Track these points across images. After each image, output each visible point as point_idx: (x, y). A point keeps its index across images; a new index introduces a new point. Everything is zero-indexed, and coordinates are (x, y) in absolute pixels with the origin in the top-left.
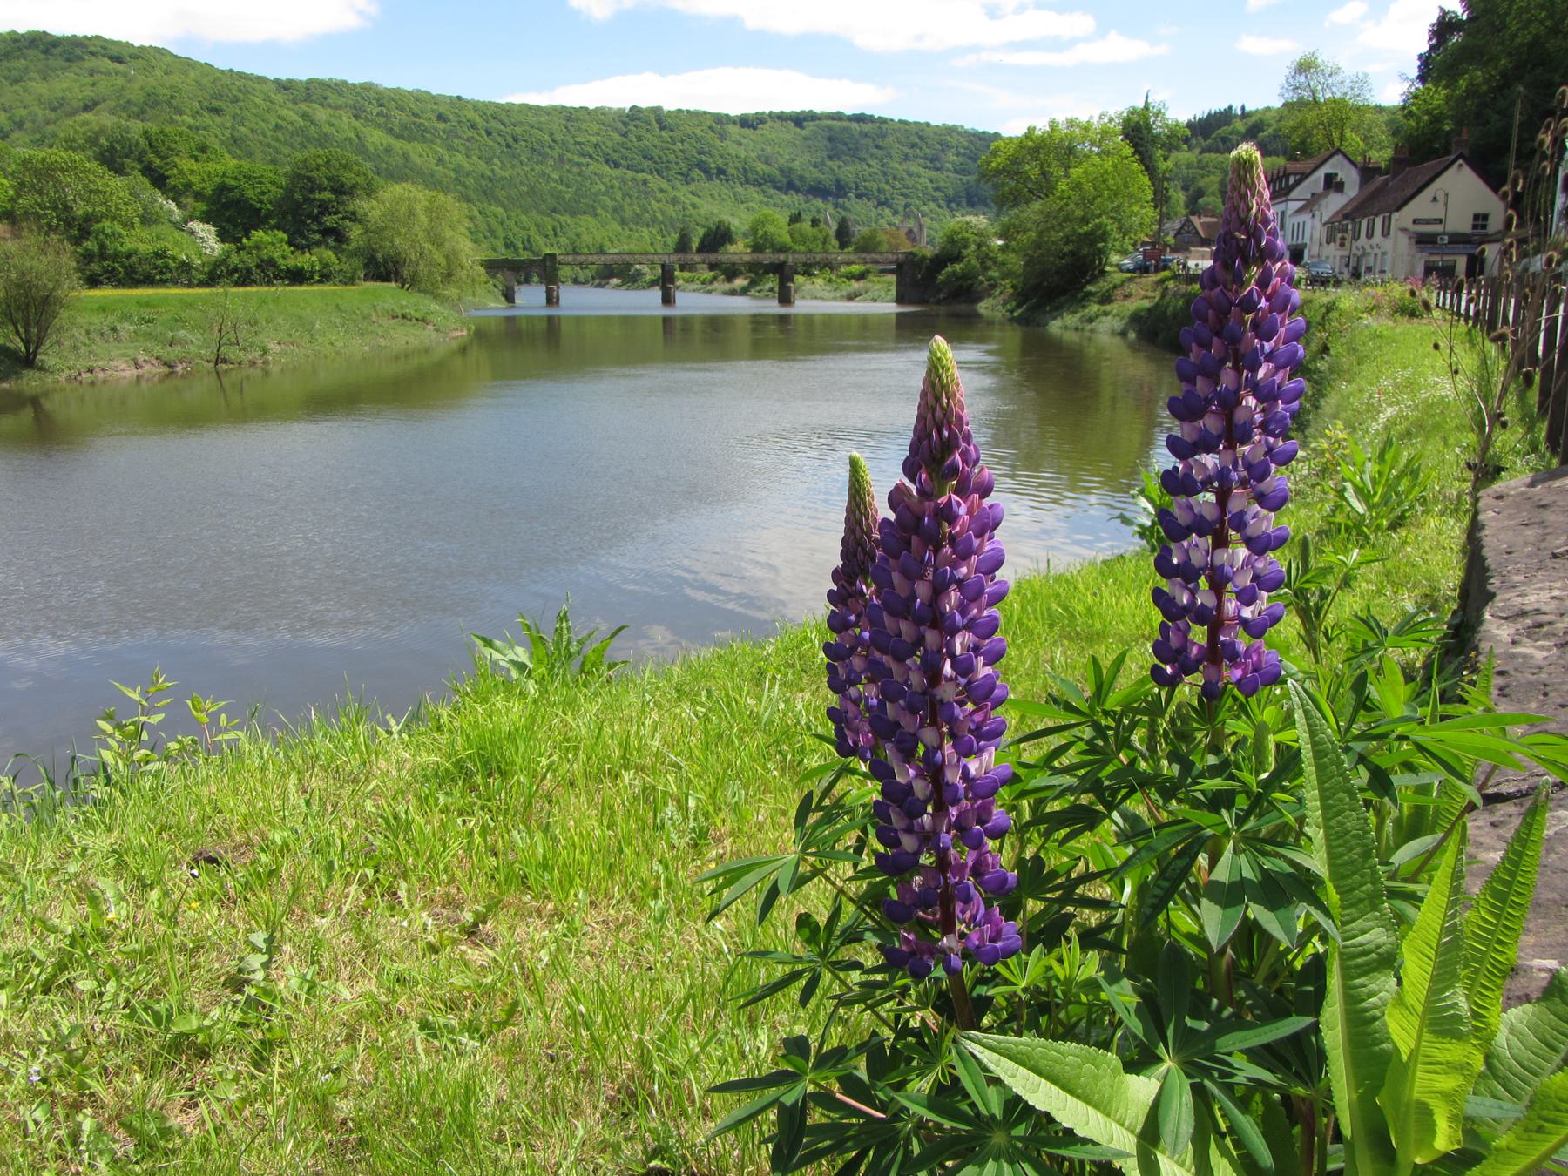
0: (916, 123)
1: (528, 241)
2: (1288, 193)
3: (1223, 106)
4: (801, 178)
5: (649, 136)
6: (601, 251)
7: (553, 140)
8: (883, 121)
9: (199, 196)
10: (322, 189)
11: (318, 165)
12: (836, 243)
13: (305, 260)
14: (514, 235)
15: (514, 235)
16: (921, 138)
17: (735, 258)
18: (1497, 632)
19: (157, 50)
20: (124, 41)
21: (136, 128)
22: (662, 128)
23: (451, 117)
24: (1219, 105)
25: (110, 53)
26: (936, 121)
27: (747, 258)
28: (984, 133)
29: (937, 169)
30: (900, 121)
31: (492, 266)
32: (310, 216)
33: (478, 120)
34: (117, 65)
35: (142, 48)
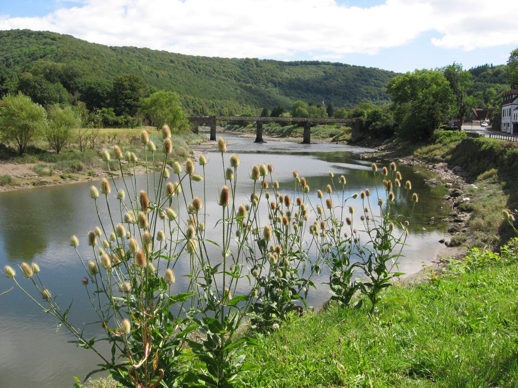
0: (359, 67)
1: (203, 109)
2: (512, 102)
3: (484, 64)
4: (312, 87)
5: (252, 69)
6: (231, 114)
7: (214, 70)
8: (346, 66)
9: (81, 91)
10: (126, 90)
11: (126, 80)
12: (327, 114)
13: (121, 119)
14: (197, 107)
15: (197, 107)
16: (361, 72)
17: (286, 119)
18: (366, 116)
19: (68, 36)
20: (57, 32)
21: (60, 66)
22: (257, 67)
23: (176, 61)
24: (482, 63)
25: (51, 37)
26: (368, 66)
27: (291, 119)
28: (387, 71)
29: (368, 85)
30: (353, 66)
31: (192, 120)
32: (121, 99)
33: (186, 63)
34: (53, 41)
35: (63, 35)
